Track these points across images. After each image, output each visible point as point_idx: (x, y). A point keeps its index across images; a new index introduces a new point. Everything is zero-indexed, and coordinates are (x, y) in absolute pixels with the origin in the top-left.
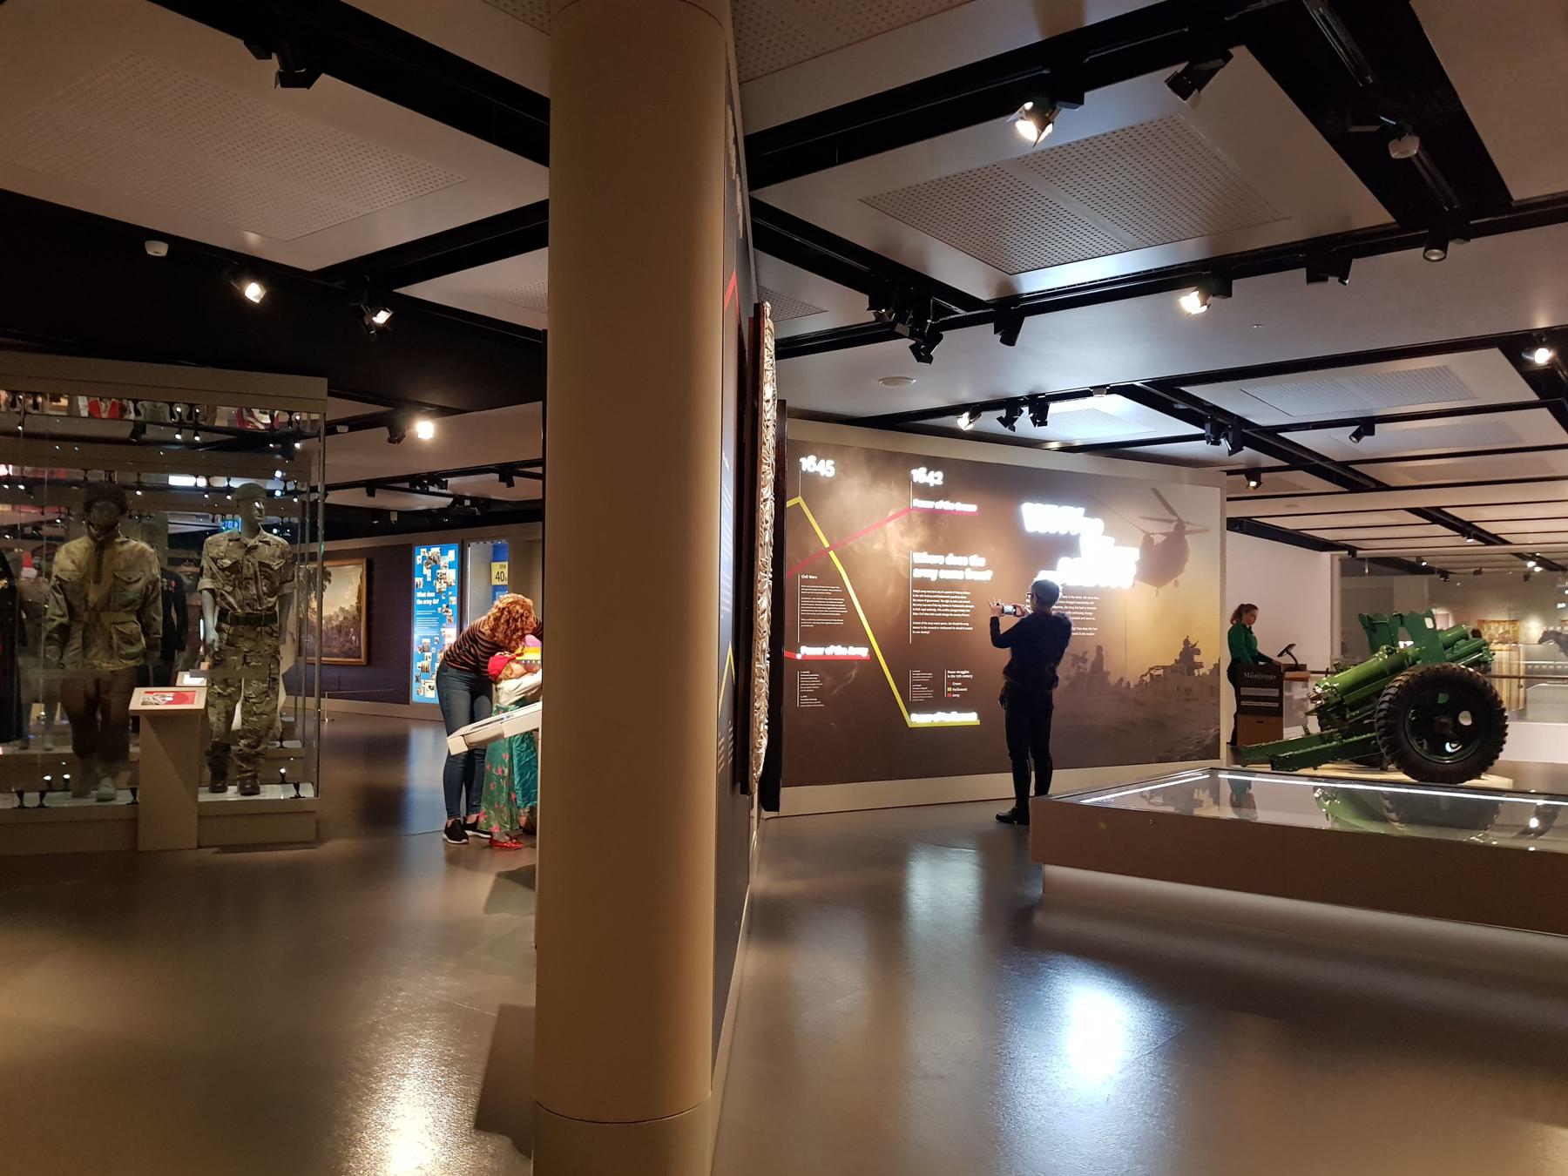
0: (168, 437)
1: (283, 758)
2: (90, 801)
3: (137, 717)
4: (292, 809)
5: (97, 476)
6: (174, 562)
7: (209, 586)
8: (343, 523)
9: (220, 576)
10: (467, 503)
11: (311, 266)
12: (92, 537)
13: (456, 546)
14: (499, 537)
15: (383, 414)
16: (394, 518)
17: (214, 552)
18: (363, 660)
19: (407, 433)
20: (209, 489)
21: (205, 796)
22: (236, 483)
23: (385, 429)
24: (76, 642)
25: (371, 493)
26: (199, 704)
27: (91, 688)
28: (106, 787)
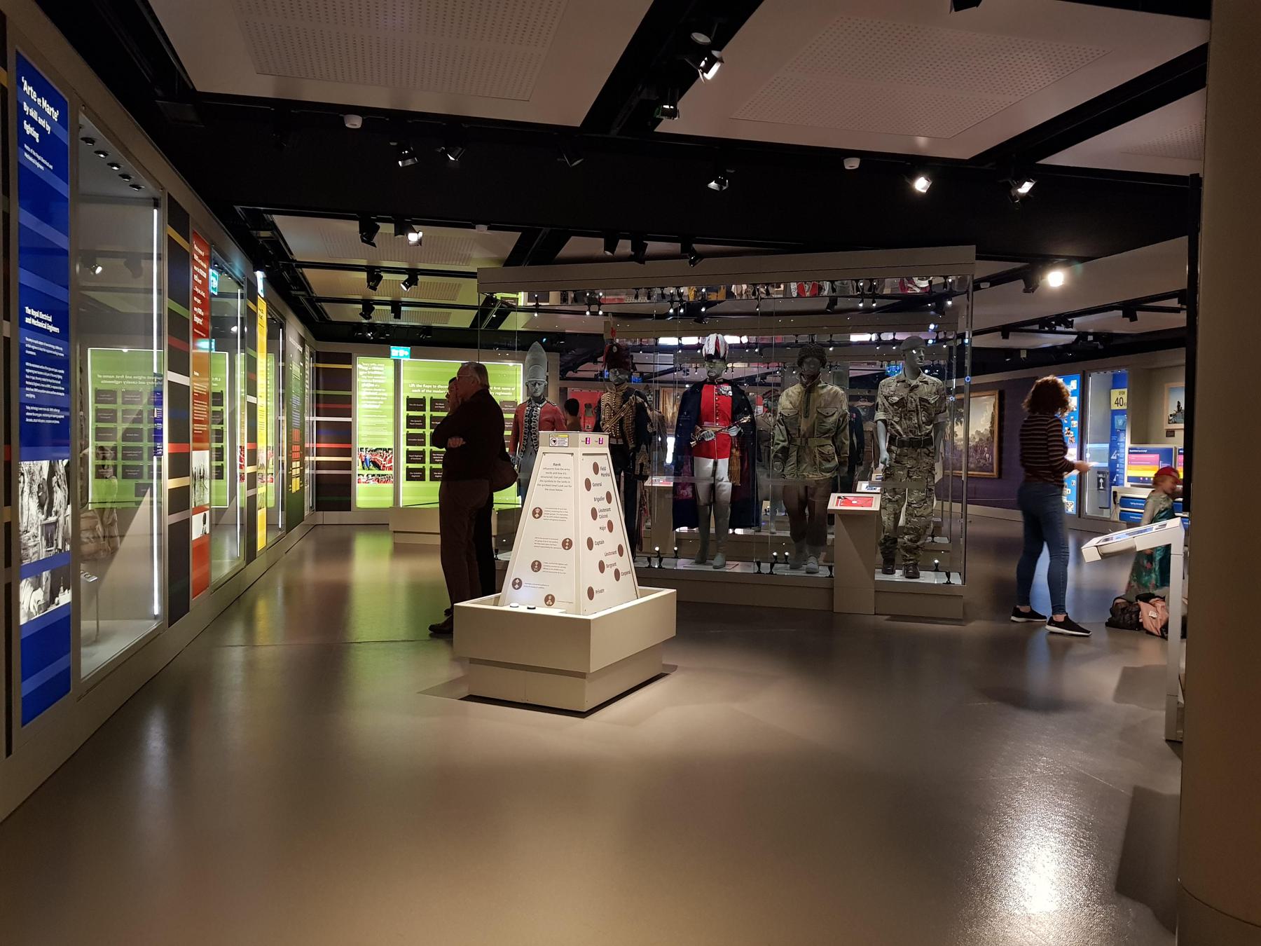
0: (851, 306)
1: (936, 551)
2: (801, 573)
3: (831, 516)
4: (944, 593)
5: (804, 339)
6: (857, 398)
7: (883, 417)
8: (985, 361)
9: (891, 409)
10: (1090, 338)
11: (967, 155)
12: (804, 385)
13: (1078, 376)
14: (1119, 367)
15: (1020, 269)
16: (1024, 355)
17: (886, 391)
18: (995, 473)
19: (1041, 282)
20: (879, 342)
21: (880, 576)
22: (900, 336)
23: (1022, 281)
24: (793, 459)
25: (1005, 336)
26: (876, 506)
27: (802, 492)
28: (812, 563)
